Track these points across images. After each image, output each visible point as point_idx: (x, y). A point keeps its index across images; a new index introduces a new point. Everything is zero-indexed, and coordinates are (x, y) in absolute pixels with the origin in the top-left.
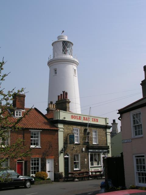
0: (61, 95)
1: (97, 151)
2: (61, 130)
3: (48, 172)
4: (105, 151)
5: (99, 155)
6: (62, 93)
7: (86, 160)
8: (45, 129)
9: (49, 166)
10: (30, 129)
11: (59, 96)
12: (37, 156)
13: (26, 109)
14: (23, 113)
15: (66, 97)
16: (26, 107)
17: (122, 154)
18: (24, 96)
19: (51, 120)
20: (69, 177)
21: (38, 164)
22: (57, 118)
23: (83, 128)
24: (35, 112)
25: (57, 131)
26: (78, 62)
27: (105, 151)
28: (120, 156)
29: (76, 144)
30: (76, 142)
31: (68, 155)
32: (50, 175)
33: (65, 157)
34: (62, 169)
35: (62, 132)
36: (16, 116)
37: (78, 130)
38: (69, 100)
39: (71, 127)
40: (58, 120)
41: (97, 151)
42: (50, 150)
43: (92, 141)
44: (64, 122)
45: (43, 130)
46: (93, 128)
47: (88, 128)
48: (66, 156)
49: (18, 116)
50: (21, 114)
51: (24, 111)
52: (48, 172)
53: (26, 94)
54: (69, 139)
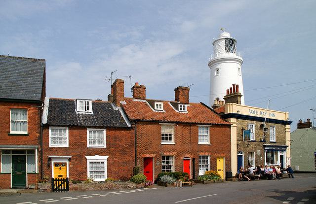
0: (231, 88)
1: (274, 149)
2: (234, 125)
3: (219, 170)
4: (283, 149)
5: (276, 154)
6: (232, 87)
7: (261, 158)
8: (215, 124)
9: (221, 164)
10: (198, 124)
11: (228, 91)
12: (206, 154)
13: (191, 104)
14: (188, 107)
15: (237, 91)
16: (190, 102)
17: (308, 120)
18: (188, 90)
19: (221, 114)
20: (244, 175)
21: (207, 162)
22: (230, 111)
23: (259, 123)
24: (202, 106)
25: (229, 126)
26: (242, 60)
27: (283, 149)
28: (307, 121)
29: (252, 141)
30: (251, 140)
31: (241, 153)
32: (222, 175)
33: (238, 154)
34: (234, 171)
35: (236, 128)
36: (179, 110)
37: (254, 126)
38: (240, 93)
39: (246, 122)
40: (230, 114)
41: (274, 149)
42: (221, 147)
43: (269, 138)
44: (238, 116)
45: (214, 125)
46: (270, 124)
47: (265, 124)
48: (239, 154)
49: (183, 111)
50: (186, 108)
51: (189, 105)
52: (219, 170)
53: (190, 88)
54: (244, 134)
